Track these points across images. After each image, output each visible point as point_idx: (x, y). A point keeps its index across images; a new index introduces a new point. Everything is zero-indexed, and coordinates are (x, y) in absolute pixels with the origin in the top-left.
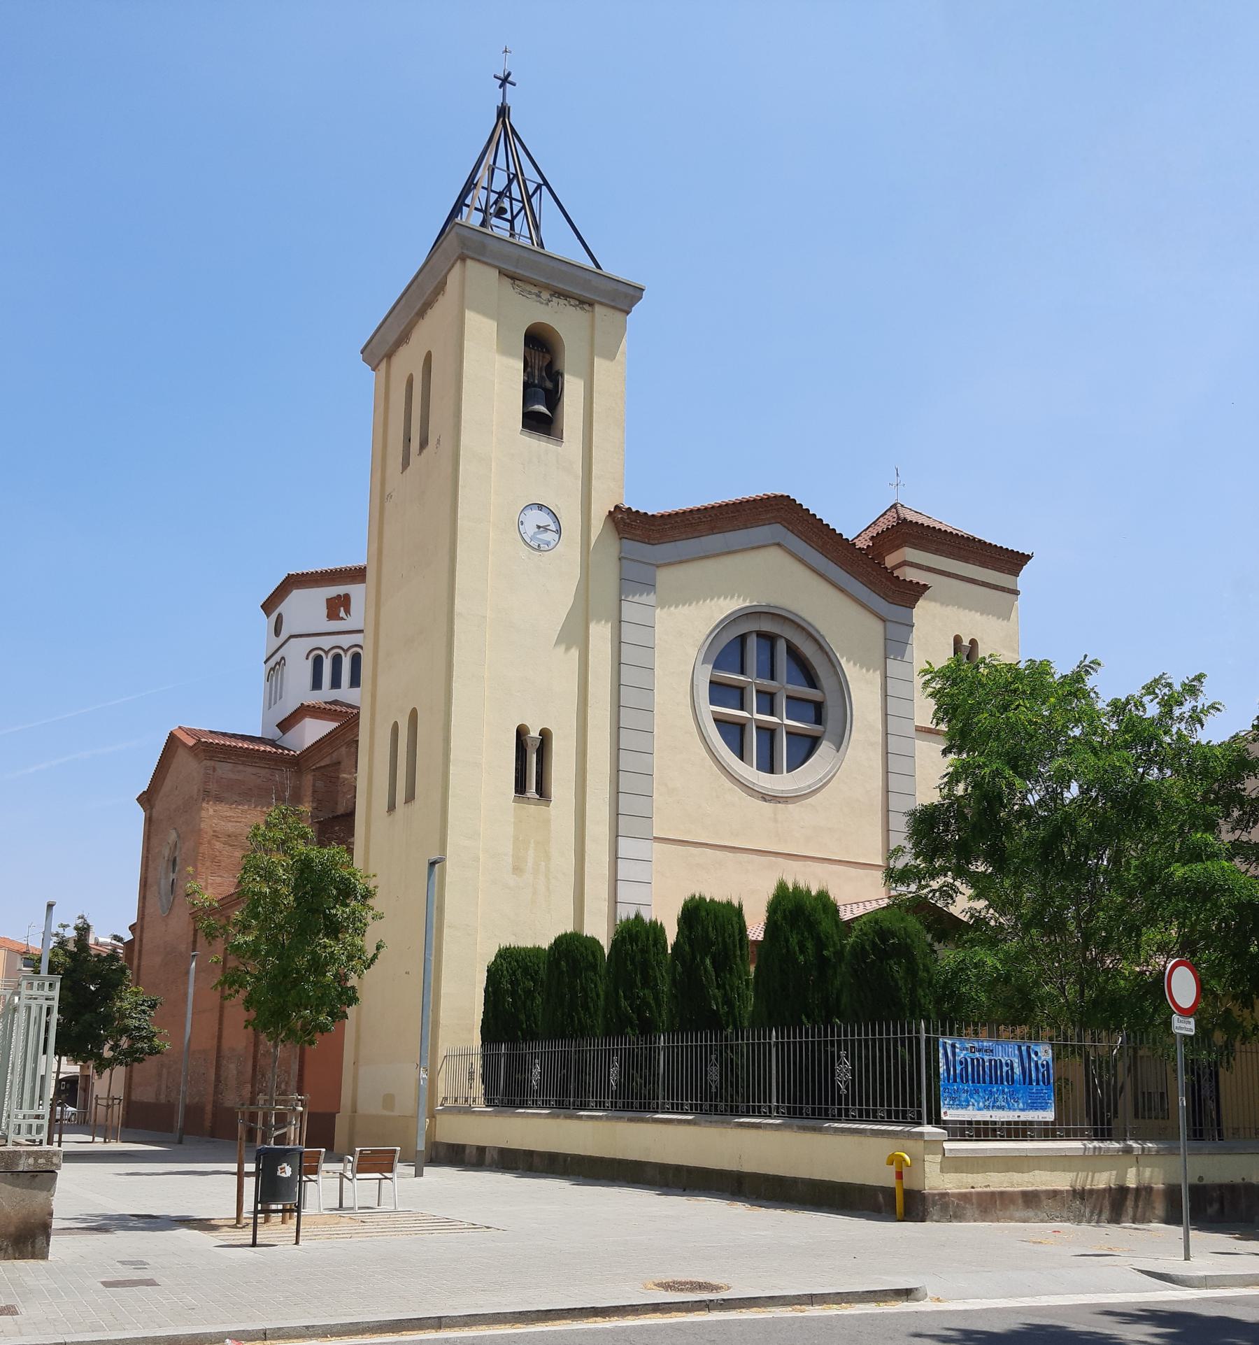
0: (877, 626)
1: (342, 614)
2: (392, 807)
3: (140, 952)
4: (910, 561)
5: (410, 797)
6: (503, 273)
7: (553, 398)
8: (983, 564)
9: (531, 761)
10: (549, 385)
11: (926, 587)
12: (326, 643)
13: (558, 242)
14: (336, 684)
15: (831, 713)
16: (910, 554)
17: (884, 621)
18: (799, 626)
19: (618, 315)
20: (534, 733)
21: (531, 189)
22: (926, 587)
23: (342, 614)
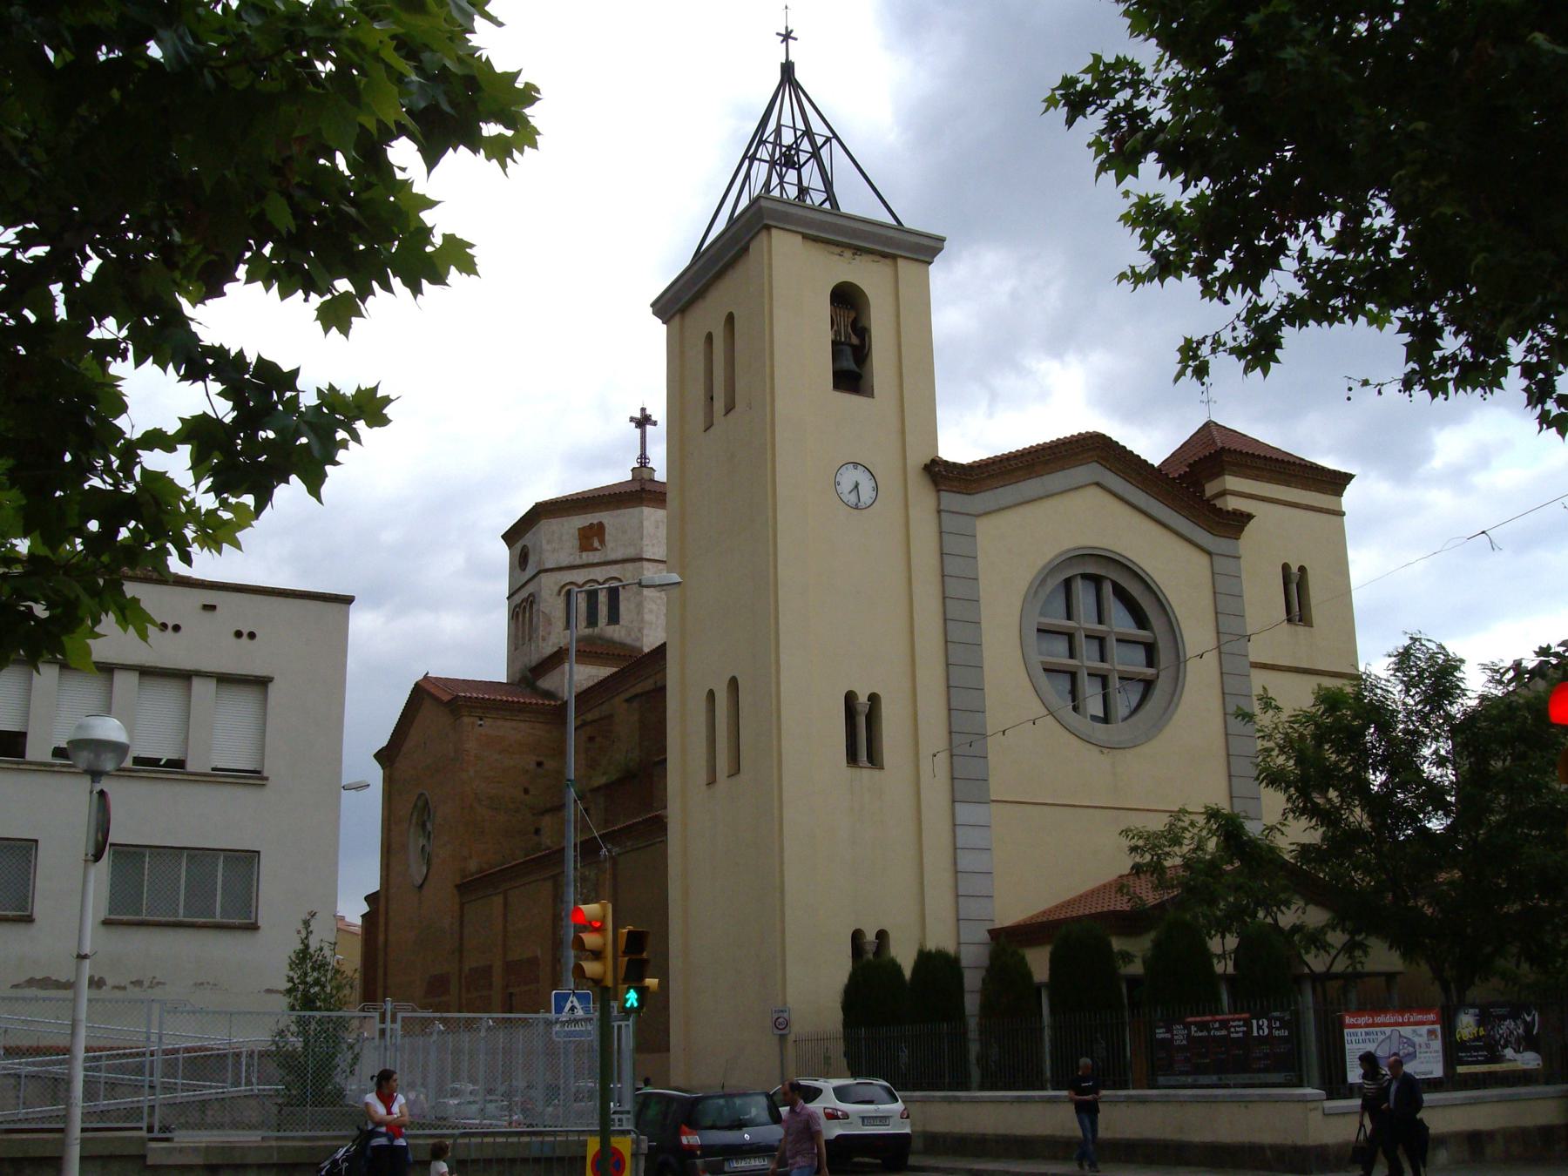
0: (1204, 560)
1: (596, 544)
2: (712, 781)
3: (386, 924)
4: (1236, 490)
5: (736, 770)
6: (805, 237)
7: (861, 352)
8: (1306, 487)
9: (862, 728)
10: (855, 340)
11: (1250, 517)
12: (579, 576)
13: (855, 201)
14: (592, 620)
15: (1165, 656)
16: (1232, 482)
17: (1210, 554)
18: (1159, 600)
19: (923, 266)
20: (863, 698)
21: (820, 141)
22: (1250, 517)
23: (596, 544)
